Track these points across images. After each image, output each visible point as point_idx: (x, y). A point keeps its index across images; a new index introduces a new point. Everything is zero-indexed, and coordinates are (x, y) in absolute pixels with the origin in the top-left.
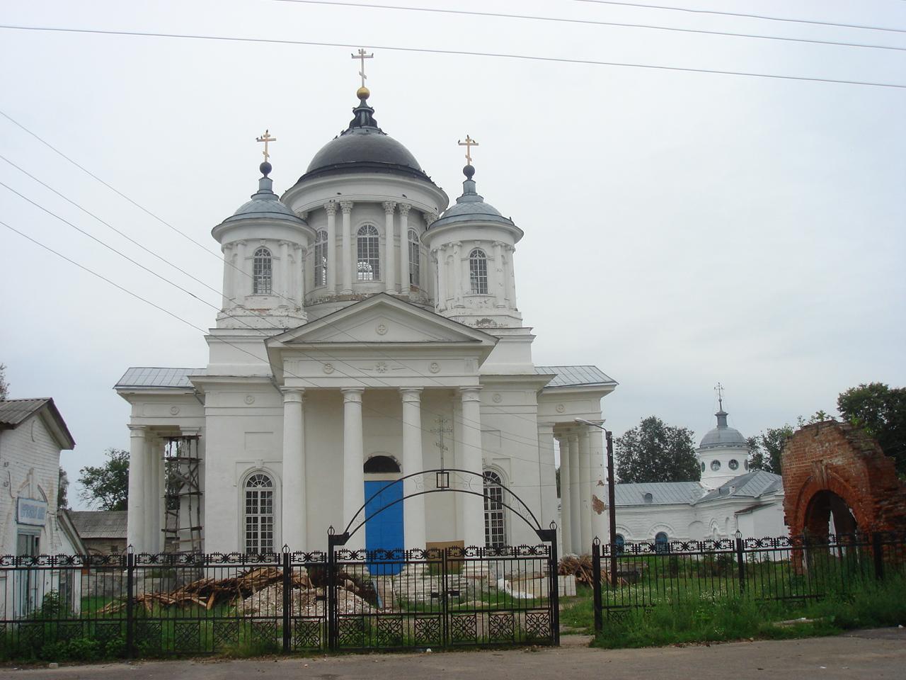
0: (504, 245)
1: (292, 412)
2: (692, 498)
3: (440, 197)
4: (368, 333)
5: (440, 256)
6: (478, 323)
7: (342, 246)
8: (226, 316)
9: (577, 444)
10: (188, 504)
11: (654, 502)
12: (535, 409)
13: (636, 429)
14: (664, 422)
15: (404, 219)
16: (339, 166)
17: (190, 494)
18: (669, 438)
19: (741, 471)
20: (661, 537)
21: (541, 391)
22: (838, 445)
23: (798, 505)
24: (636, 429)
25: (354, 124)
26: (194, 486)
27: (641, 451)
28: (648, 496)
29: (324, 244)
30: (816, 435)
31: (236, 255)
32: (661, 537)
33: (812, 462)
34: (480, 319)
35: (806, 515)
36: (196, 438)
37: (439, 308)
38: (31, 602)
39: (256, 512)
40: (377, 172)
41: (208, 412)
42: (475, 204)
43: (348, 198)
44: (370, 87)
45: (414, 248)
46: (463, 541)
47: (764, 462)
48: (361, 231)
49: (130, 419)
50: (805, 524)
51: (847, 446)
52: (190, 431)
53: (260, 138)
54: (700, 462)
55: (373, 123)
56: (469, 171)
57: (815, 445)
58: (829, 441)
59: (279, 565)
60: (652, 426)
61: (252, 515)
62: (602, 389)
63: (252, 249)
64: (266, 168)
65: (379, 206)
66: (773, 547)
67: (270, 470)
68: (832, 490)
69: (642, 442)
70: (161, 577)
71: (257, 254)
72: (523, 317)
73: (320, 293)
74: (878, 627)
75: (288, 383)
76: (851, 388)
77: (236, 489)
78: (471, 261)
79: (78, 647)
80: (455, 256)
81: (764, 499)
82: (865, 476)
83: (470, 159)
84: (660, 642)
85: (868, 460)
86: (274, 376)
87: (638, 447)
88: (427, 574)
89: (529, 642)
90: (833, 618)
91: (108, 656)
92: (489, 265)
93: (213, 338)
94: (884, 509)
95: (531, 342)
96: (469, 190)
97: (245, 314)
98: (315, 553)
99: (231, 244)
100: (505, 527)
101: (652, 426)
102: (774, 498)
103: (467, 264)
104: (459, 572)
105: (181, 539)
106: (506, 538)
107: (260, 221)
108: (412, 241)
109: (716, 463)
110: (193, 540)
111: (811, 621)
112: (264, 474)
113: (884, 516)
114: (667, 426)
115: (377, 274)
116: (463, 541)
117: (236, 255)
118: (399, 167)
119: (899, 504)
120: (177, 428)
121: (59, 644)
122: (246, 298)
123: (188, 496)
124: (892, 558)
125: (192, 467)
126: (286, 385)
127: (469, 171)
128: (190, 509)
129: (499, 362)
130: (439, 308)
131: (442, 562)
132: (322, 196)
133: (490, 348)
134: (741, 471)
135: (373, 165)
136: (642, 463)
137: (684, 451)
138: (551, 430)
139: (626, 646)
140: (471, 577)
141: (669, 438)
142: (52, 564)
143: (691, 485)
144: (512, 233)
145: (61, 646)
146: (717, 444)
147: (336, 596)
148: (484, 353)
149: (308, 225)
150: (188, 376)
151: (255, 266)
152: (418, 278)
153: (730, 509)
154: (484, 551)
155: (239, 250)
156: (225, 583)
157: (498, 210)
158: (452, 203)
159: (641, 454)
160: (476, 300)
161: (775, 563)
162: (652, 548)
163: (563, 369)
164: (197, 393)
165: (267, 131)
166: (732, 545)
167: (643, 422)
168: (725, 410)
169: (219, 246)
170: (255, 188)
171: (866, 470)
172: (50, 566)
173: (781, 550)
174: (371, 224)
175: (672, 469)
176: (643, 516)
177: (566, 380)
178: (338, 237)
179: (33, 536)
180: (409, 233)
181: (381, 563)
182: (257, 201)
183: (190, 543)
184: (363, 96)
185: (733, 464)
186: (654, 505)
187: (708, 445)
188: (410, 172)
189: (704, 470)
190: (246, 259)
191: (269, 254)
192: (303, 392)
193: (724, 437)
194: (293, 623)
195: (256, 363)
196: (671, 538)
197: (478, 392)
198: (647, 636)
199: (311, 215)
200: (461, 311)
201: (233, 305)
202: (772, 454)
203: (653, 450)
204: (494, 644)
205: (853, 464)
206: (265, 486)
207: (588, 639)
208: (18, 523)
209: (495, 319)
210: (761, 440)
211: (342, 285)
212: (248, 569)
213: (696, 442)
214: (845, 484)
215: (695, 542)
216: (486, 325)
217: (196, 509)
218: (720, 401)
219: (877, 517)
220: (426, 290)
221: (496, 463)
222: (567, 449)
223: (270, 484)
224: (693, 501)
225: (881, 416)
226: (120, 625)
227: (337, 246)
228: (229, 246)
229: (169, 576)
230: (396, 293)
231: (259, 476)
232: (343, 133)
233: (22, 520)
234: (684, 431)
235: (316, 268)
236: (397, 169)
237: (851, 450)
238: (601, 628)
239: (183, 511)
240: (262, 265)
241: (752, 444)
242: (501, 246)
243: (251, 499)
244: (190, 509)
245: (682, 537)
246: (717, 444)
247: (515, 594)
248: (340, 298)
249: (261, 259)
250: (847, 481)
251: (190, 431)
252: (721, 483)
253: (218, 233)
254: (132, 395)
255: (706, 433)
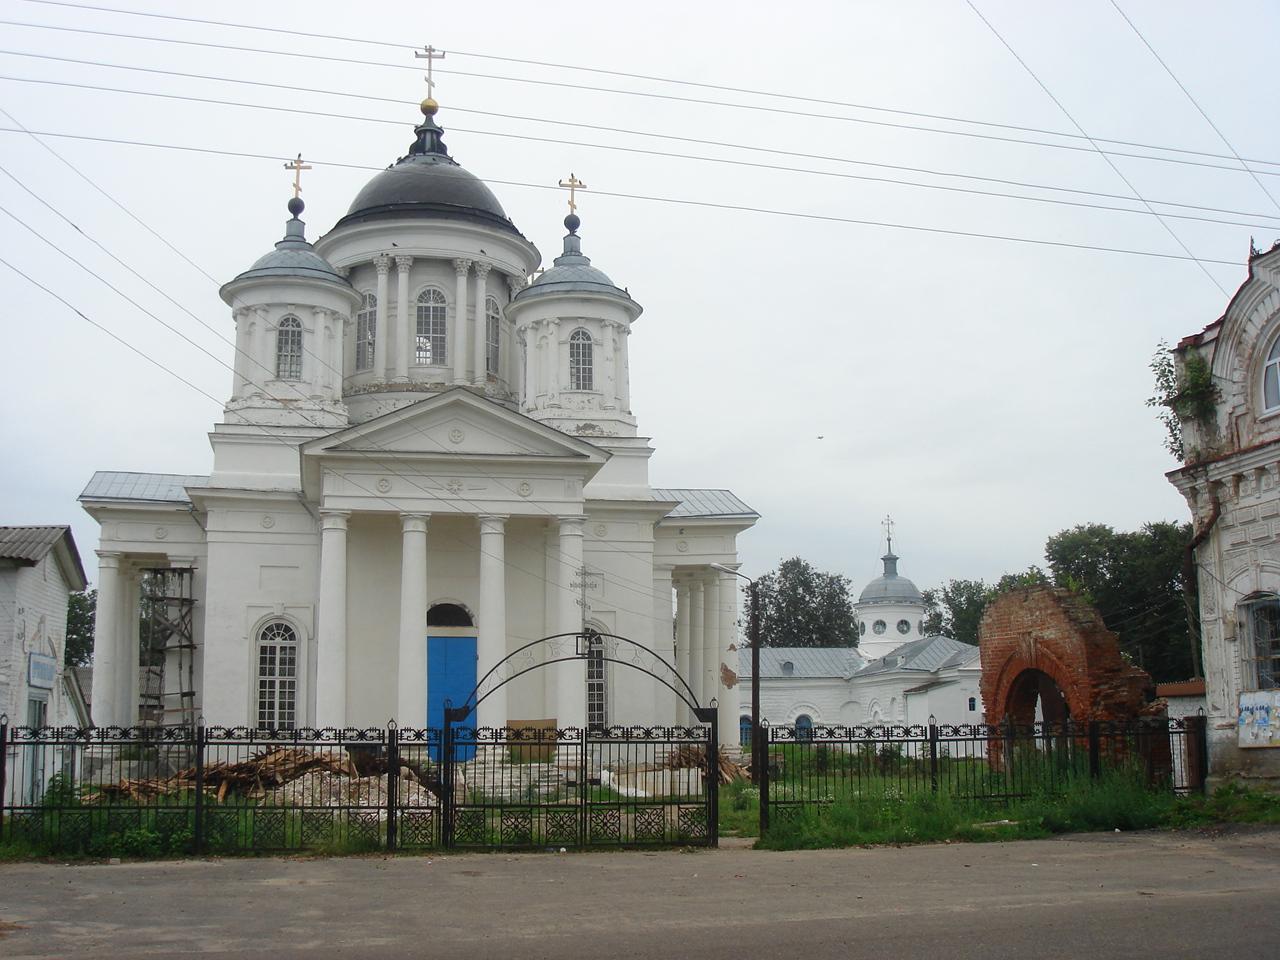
0: (616, 325)
1: (334, 541)
2: (846, 670)
3: (531, 256)
4: (438, 439)
5: (530, 336)
6: (578, 428)
7: (396, 316)
8: (237, 407)
9: (702, 594)
10: (178, 662)
11: (796, 673)
12: (650, 547)
13: (774, 574)
14: (811, 566)
15: (482, 284)
16: (396, 208)
17: (181, 647)
18: (817, 587)
19: (914, 636)
20: (803, 721)
21: (658, 523)
22: (1052, 614)
23: (998, 686)
24: (774, 574)
25: (416, 149)
26: (186, 637)
27: (779, 604)
28: (788, 666)
29: (371, 313)
30: (1025, 601)
31: (253, 323)
32: (803, 721)
33: (1019, 634)
34: (581, 424)
35: (1008, 698)
36: (190, 570)
37: (526, 406)
38: (38, 786)
39: (272, 673)
40: (447, 218)
41: (210, 537)
42: (579, 267)
43: (407, 252)
44: (438, 98)
45: (493, 322)
46: (556, 720)
47: (943, 624)
48: (423, 297)
49: (98, 542)
50: (1007, 709)
51: (1062, 616)
52: (180, 561)
53: (289, 165)
54: (859, 620)
55: (442, 149)
56: (572, 223)
57: (1022, 613)
58: (1040, 609)
59: (384, 744)
60: (794, 570)
61: (267, 678)
62: (743, 520)
63: (275, 317)
64: (296, 207)
65: (448, 264)
66: (973, 737)
67: (300, 622)
68: (1041, 668)
69: (781, 592)
70: (139, 759)
71: (282, 324)
72: (637, 423)
73: (363, 379)
74: (1092, 830)
75: (328, 504)
76: (1065, 530)
77: (247, 642)
78: (572, 345)
79: (137, 841)
80: (549, 337)
81: (944, 675)
82: (1082, 653)
83: (573, 207)
84: (841, 843)
85: (1086, 634)
86: (303, 491)
87: (775, 598)
88: (507, 762)
89: (681, 842)
90: (1041, 819)
91: (173, 852)
92: (596, 352)
93: (217, 438)
94: (1102, 694)
95: (649, 457)
96: (572, 248)
97: (264, 405)
98: (370, 730)
99: (248, 309)
100: (606, 703)
101: (794, 570)
102: (957, 674)
103: (567, 348)
104: (549, 760)
105: (165, 708)
106: (606, 718)
107: (289, 280)
108: (491, 313)
109: (881, 625)
110: (184, 710)
111: (1016, 823)
112: (285, 623)
113: (1103, 703)
114: (815, 571)
115: (439, 353)
116: (556, 720)
117: (253, 323)
118: (477, 212)
119: (1122, 689)
120: (163, 556)
121: (113, 836)
122: (266, 384)
123: (178, 649)
124: (1110, 753)
125: (185, 610)
126: (326, 506)
127: (572, 223)
128: (181, 668)
129: (607, 484)
130: (526, 406)
131: (581, 744)
132: (371, 246)
133: (597, 467)
134: (914, 636)
135: (441, 208)
136: (780, 621)
137: (836, 606)
138: (668, 576)
139: (801, 847)
140: (563, 768)
141: (817, 587)
142: (103, 738)
143: (844, 652)
144: (627, 309)
145: (114, 839)
146: (883, 599)
147: (452, 782)
148: (590, 470)
149: (351, 286)
150: (186, 488)
151: (280, 341)
152: (497, 364)
153: (896, 686)
154: (344, 733)
155: (258, 318)
156: (239, 768)
157: (610, 278)
158: (547, 264)
159: (779, 609)
160: (578, 398)
161: (958, 760)
162: (792, 733)
163: (686, 493)
164: (194, 509)
165: (300, 155)
166: (924, 732)
167: (783, 565)
168: (895, 553)
169: (229, 310)
170: (281, 234)
171: (1083, 647)
172: (100, 740)
173: (981, 739)
174: (438, 290)
175: (820, 630)
176: (779, 693)
177: (691, 509)
178: (392, 304)
179: (40, 702)
180: (488, 301)
181: (597, 742)
182: (285, 251)
183: (180, 714)
184: (429, 110)
185: (903, 626)
186: (796, 679)
187: (871, 599)
188: (493, 220)
189: (863, 632)
190: (267, 330)
191: (299, 325)
192: (349, 517)
193: (892, 590)
194: (399, 813)
195: (283, 472)
196: (817, 723)
197: (581, 523)
198: (826, 836)
199: (353, 273)
200: (556, 412)
201: (251, 390)
202: (955, 614)
203: (796, 603)
204: (639, 844)
205: (1068, 637)
206: (285, 639)
207: (752, 841)
208: (30, 685)
209: (601, 425)
210: (941, 595)
211: (394, 369)
212: (263, 749)
213: (854, 595)
214: (1058, 662)
215: (332, 730)
216: (588, 432)
217: (188, 669)
218: (889, 540)
219: (1094, 704)
220: (508, 382)
221: (598, 616)
222: (688, 601)
223: (292, 637)
224: (848, 675)
225: (1102, 568)
226: (186, 813)
227: (389, 317)
228: (245, 312)
229: (148, 758)
230: (468, 384)
231: (278, 626)
232: (400, 161)
233: (35, 681)
234: (838, 578)
235: (358, 345)
236: (475, 215)
237: (1067, 620)
238: (768, 827)
239: (171, 669)
240: (290, 339)
241: (928, 599)
242: (613, 327)
243: (266, 657)
244: (181, 668)
245: (828, 722)
246: (883, 599)
247: (623, 791)
248: (392, 388)
249: (287, 332)
250: (1060, 658)
251: (180, 561)
252: (885, 652)
253: (229, 293)
254: (104, 510)
255: (868, 582)
